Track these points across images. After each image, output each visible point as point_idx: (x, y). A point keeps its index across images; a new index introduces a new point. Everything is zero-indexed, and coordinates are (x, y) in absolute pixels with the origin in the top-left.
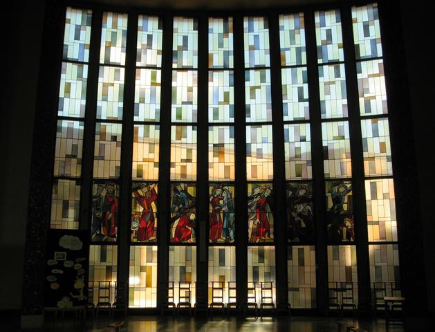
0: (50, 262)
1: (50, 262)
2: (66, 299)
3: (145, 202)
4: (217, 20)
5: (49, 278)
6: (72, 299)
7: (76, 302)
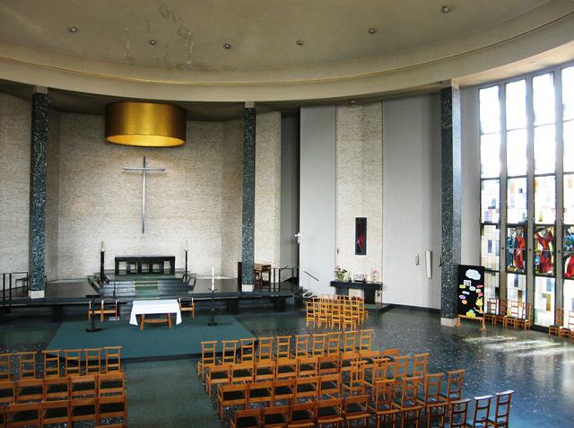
0: (461, 287)
1: (461, 287)
2: (471, 311)
3: (544, 242)
4: (63, 225)
5: (461, 297)
6: (475, 312)
7: (478, 314)
